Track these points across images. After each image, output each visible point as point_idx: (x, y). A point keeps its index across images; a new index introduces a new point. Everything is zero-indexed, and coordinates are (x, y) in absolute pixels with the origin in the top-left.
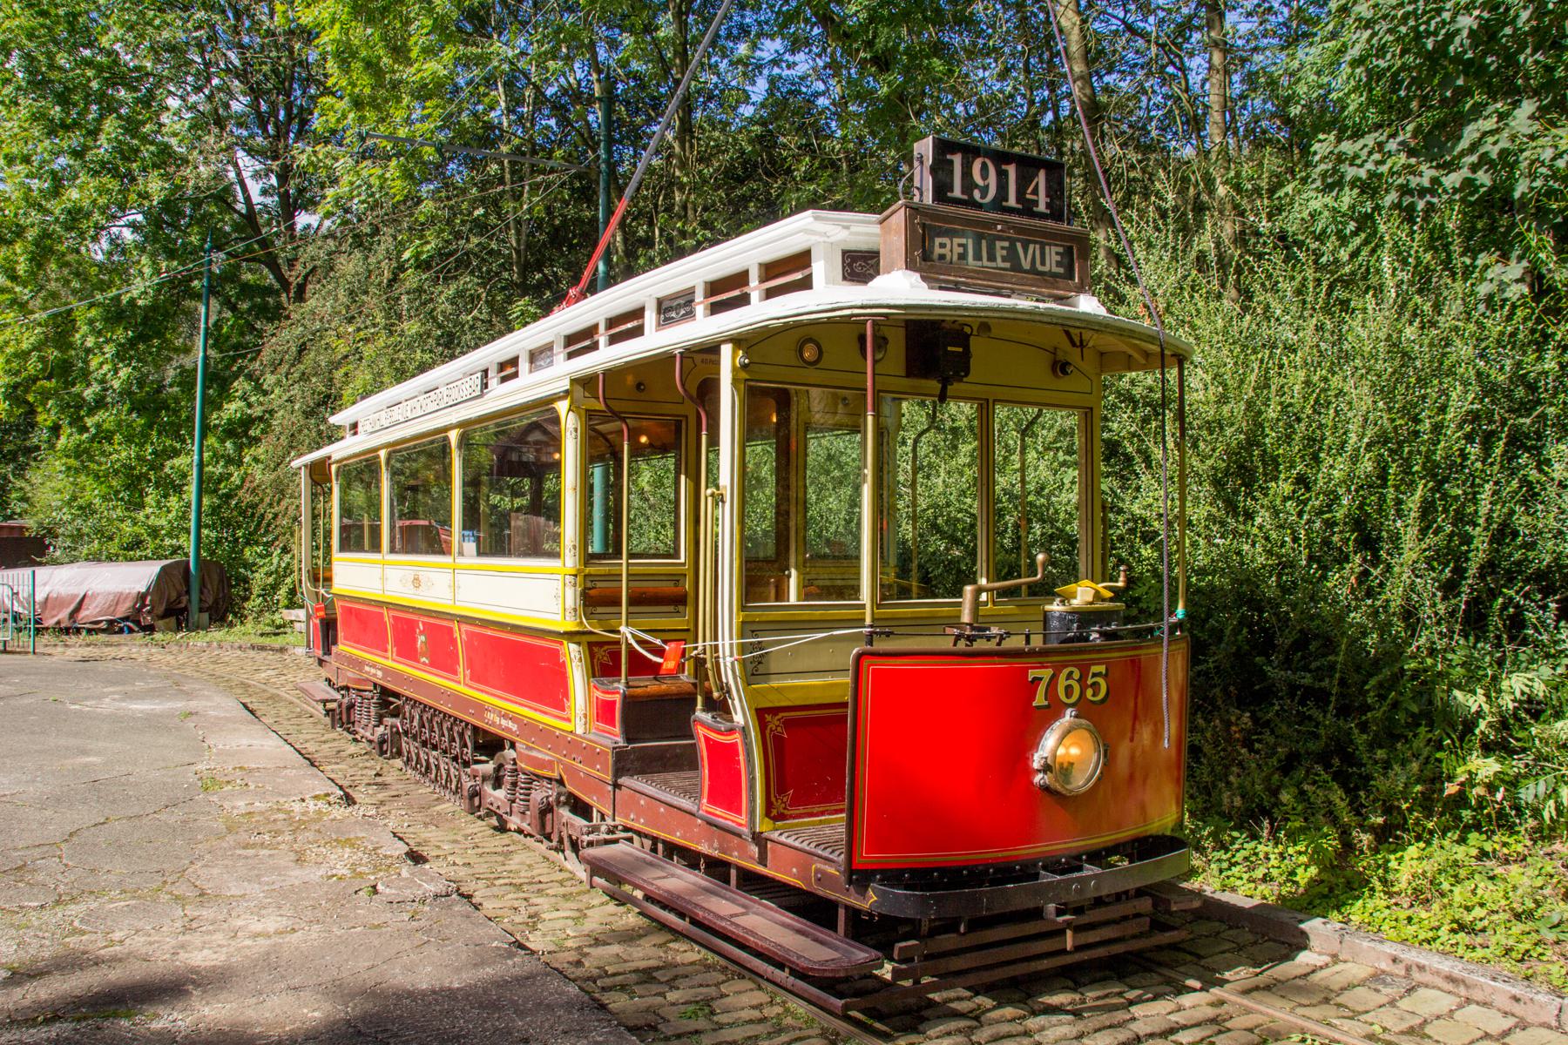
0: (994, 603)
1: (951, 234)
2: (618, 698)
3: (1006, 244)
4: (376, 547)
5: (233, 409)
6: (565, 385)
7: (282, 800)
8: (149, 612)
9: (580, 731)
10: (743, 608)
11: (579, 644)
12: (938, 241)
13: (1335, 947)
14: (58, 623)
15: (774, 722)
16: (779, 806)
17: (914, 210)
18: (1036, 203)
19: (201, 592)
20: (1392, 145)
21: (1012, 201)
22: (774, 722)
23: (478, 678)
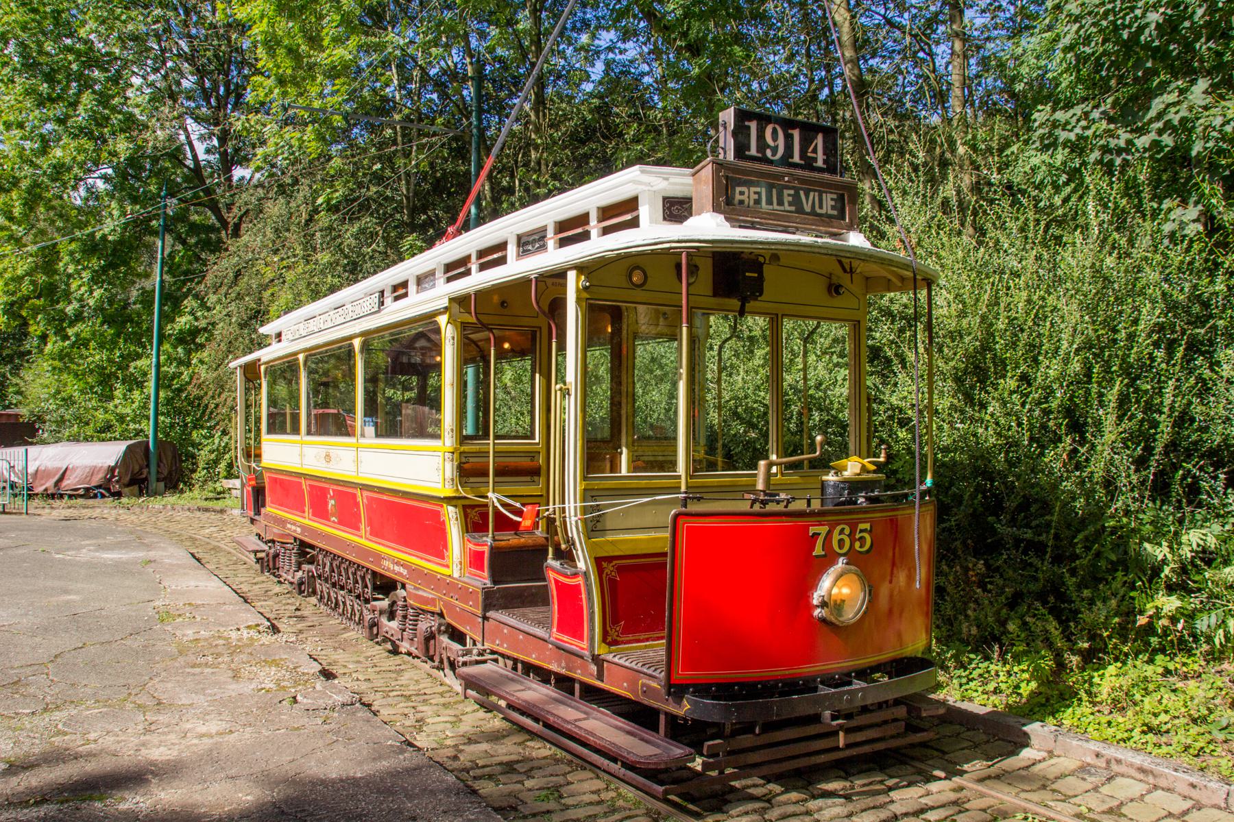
0: (782, 475)
1: (748, 184)
2: (486, 549)
3: (792, 192)
4: (296, 430)
5: (183, 321)
6: (445, 303)
7: (222, 630)
8: (117, 482)
9: (456, 575)
10: (585, 478)
11: (455, 506)
12: (738, 189)
13: (1051, 745)
14: (46, 490)
15: (609, 568)
16: (613, 634)
17: (719, 165)
18: (815, 160)
19: (159, 466)
20: (1096, 114)
21: (796, 158)
22: (609, 568)
23: (376, 533)
